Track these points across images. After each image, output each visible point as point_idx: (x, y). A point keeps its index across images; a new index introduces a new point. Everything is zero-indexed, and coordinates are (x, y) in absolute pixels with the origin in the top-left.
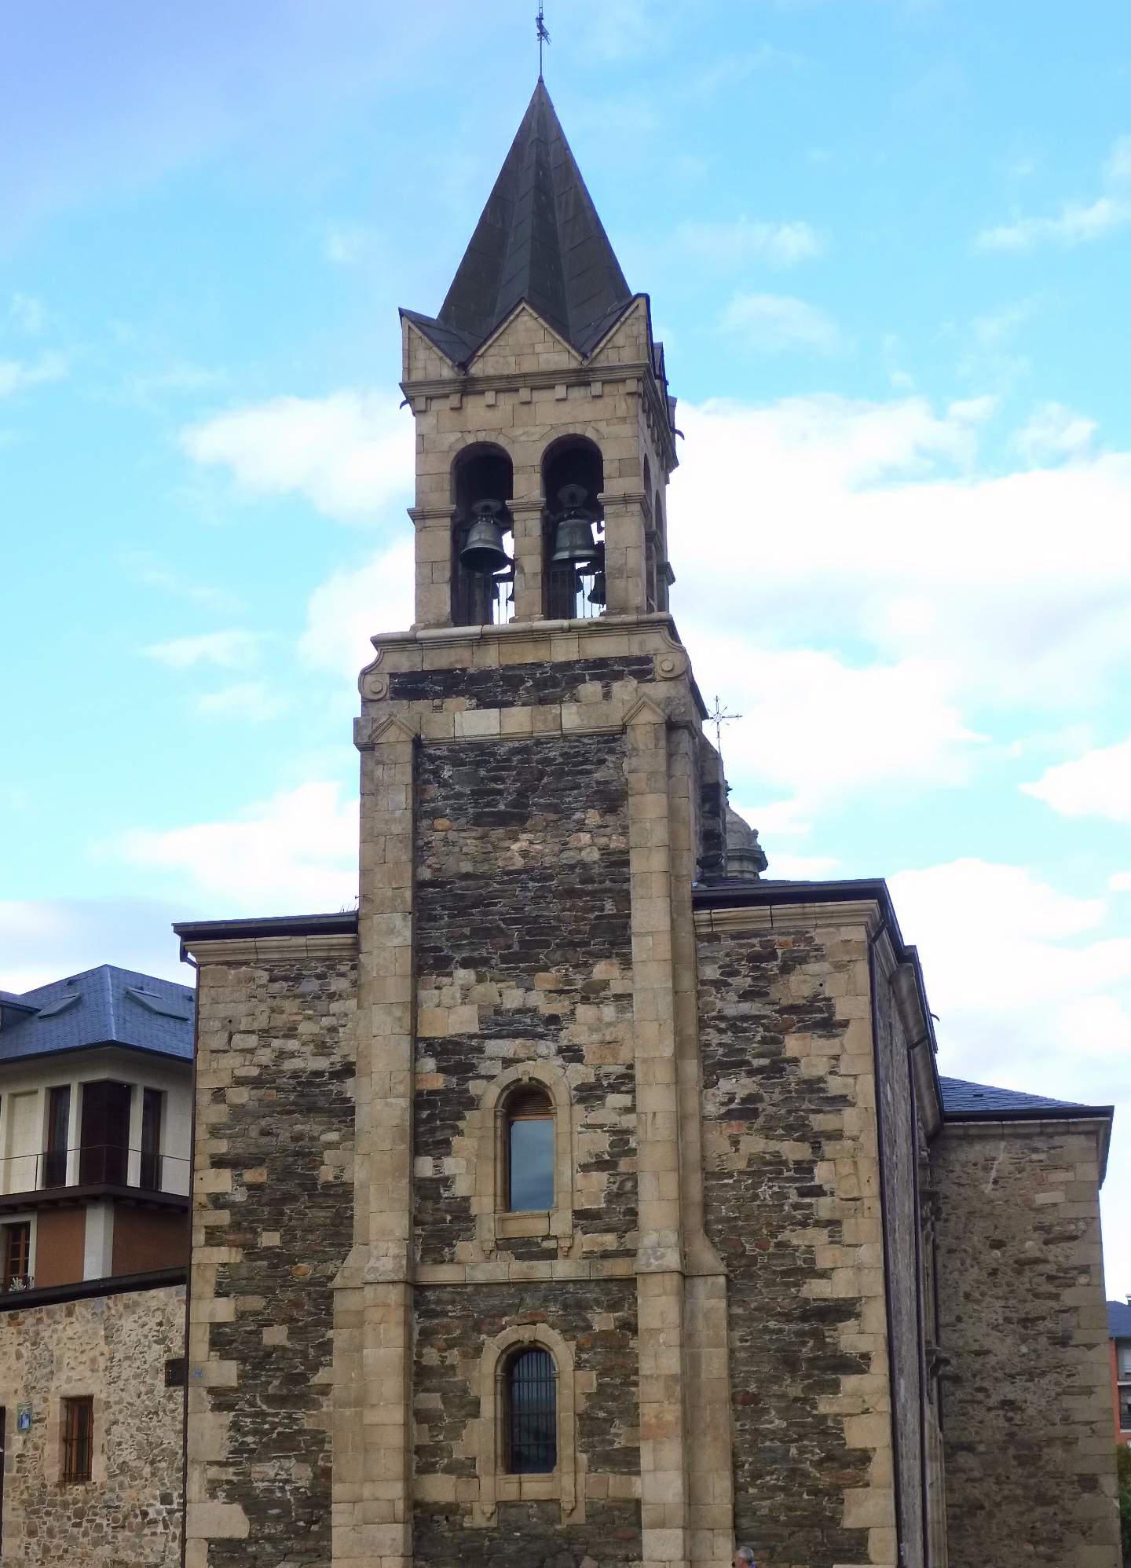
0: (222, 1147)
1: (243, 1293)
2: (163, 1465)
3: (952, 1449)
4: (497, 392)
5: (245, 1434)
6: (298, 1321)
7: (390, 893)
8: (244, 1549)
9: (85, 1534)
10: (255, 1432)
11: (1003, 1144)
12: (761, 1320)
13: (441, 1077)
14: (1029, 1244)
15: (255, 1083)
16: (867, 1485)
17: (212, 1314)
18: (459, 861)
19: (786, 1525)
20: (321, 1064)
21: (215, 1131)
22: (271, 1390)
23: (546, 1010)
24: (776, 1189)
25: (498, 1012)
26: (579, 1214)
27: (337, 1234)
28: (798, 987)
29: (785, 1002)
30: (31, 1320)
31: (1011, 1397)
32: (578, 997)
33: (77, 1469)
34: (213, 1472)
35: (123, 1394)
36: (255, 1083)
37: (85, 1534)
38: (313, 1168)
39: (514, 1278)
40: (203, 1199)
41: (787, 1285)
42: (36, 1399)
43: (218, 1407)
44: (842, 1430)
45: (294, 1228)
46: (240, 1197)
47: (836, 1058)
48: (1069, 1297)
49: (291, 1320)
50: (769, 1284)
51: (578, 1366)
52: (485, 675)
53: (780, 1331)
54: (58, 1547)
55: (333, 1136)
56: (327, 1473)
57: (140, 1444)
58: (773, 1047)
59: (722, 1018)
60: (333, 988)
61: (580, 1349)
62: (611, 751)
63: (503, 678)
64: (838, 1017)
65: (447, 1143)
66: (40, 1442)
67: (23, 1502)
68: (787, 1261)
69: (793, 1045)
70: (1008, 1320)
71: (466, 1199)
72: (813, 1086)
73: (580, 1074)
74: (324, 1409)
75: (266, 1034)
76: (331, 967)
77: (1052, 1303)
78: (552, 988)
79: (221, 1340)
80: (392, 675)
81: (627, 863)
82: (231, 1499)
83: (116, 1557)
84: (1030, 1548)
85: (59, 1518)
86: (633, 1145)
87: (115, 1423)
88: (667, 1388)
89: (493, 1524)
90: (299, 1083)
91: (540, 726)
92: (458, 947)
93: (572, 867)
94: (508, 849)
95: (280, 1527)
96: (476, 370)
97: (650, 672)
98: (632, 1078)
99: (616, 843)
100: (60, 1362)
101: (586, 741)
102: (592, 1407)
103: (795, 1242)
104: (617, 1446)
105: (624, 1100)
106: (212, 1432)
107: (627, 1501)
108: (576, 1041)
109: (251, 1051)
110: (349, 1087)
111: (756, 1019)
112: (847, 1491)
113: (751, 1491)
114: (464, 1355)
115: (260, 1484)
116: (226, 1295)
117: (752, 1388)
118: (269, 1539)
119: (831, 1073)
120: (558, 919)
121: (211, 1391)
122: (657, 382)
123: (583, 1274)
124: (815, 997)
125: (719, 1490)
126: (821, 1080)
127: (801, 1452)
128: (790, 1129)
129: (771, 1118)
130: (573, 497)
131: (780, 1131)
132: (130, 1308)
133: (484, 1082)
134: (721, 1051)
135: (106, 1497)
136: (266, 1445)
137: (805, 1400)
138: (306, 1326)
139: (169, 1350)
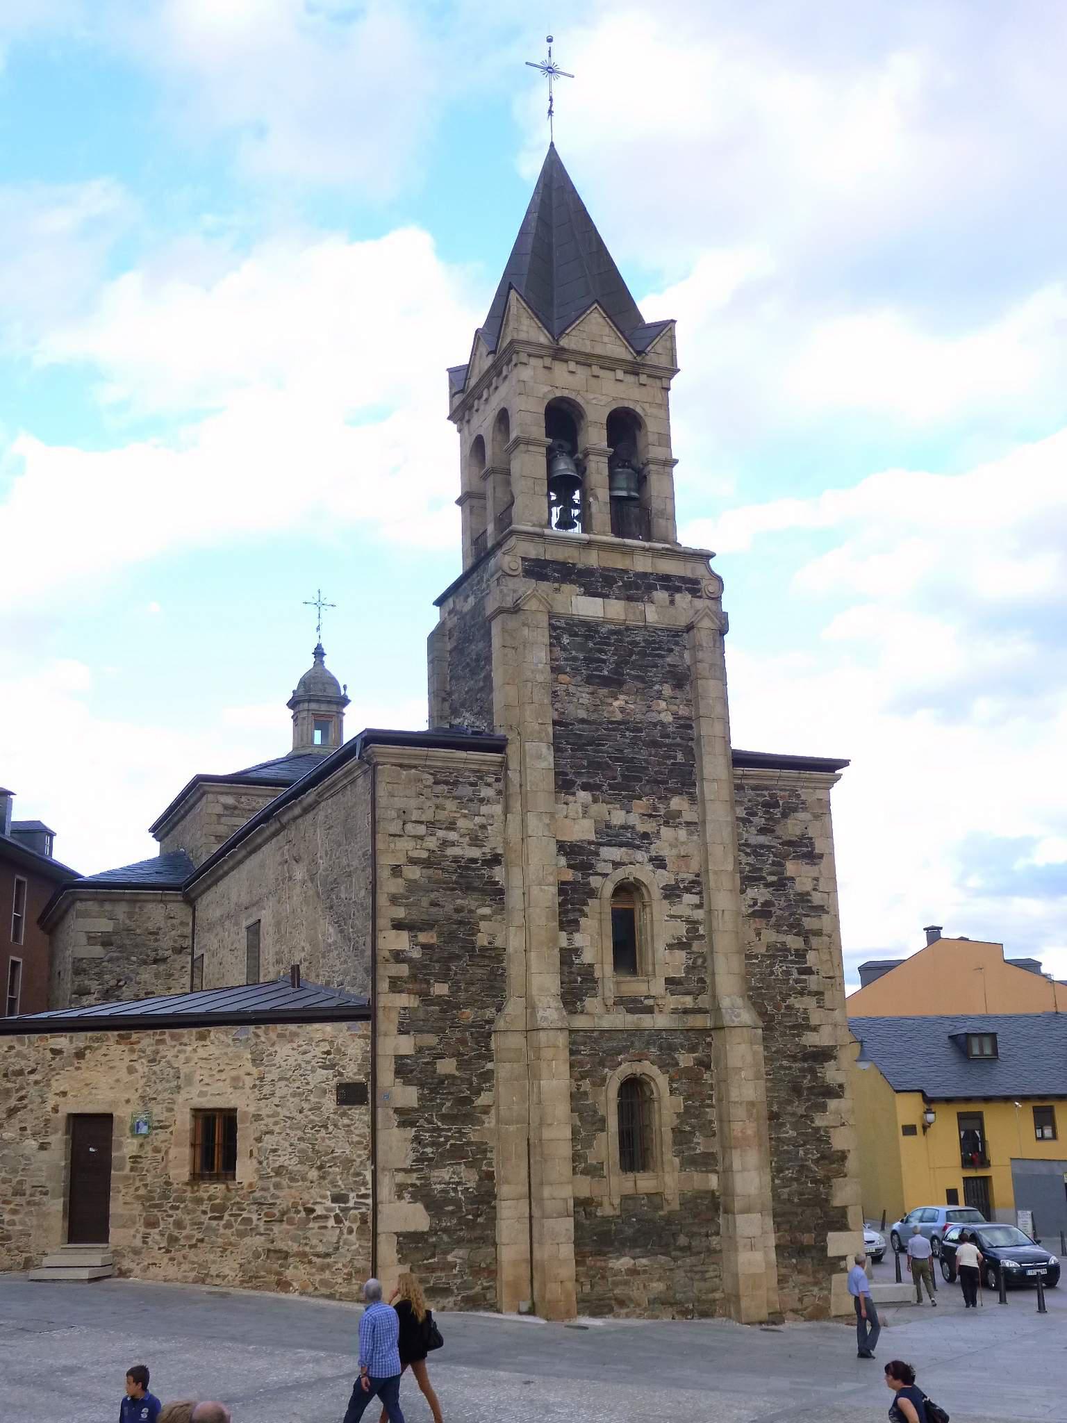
0: (400, 913)
4: (529, 355)
5: (425, 1146)
6: (463, 1055)
7: (537, 727)
8: (426, 1241)
10: (433, 1144)
12: (778, 1060)
13: (571, 871)
15: (426, 863)
16: (845, 1176)
17: (396, 1049)
18: (577, 708)
19: (799, 1205)
20: (475, 853)
21: (394, 900)
23: (641, 828)
25: (608, 826)
26: (669, 981)
27: (492, 987)
34: (400, 1177)
35: (279, 1109)
36: (426, 863)
38: (473, 935)
39: (629, 1027)
41: (794, 1036)
43: (402, 1124)
45: (458, 982)
46: (416, 954)
47: (816, 879)
49: (458, 1055)
50: (783, 1034)
51: (671, 1092)
52: (589, 572)
53: (790, 1068)
54: (188, 1237)
55: (486, 911)
56: (490, 1176)
57: (302, 1151)
58: (779, 869)
59: (747, 845)
60: (482, 795)
61: (671, 1080)
62: (677, 644)
63: (602, 575)
64: (817, 851)
65: (576, 922)
67: (138, 1197)
68: (793, 1019)
71: (591, 966)
72: (803, 897)
74: (486, 1125)
75: (431, 825)
76: (481, 778)
79: (403, 1070)
80: (524, 559)
82: (415, 1199)
83: (271, 1246)
88: (748, 1111)
89: (618, 1212)
90: (459, 867)
91: (631, 617)
92: (578, 774)
93: (655, 725)
94: (611, 705)
95: (455, 1221)
96: (564, 342)
97: (699, 590)
99: (683, 711)
102: (681, 1123)
104: (698, 1151)
106: (397, 1144)
107: (707, 1192)
108: (661, 853)
109: (421, 838)
110: (498, 873)
111: (769, 847)
114: (593, 1084)
115: (438, 1186)
116: (407, 1033)
118: (445, 1230)
119: (815, 889)
121: (396, 1110)
123: (673, 1025)
124: (803, 837)
126: (808, 894)
127: (806, 1154)
128: (791, 926)
129: (780, 918)
131: (785, 928)
133: (600, 878)
135: (257, 1194)
136: (442, 1155)
138: (471, 1059)
139: (341, 1074)
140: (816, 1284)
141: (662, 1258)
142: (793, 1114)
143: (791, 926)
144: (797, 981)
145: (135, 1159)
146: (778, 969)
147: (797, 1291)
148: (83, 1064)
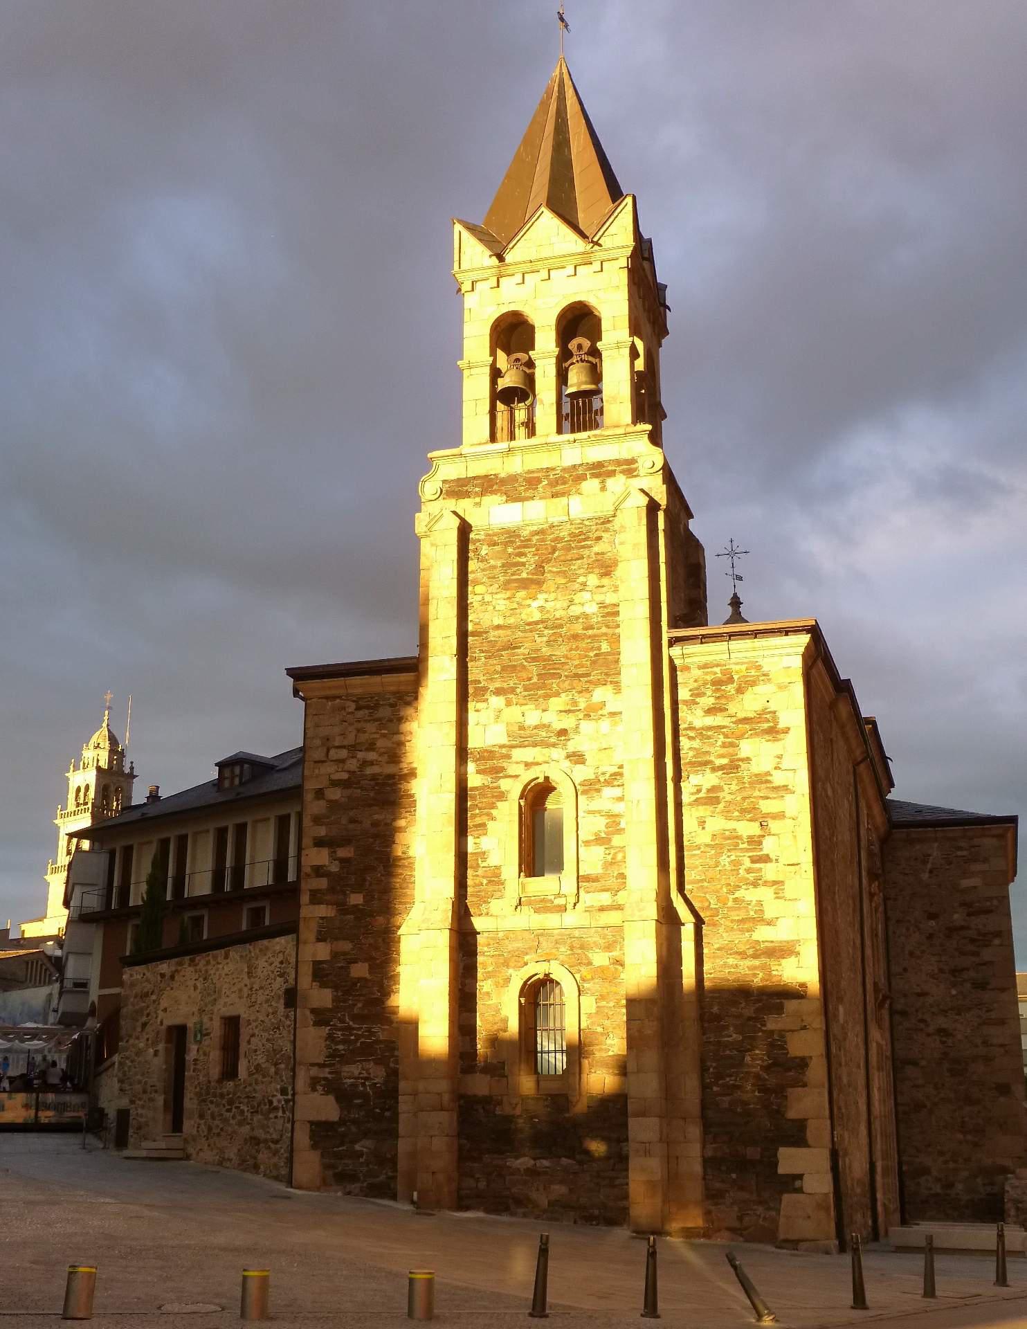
0: (322, 831)
1: (337, 939)
2: (283, 1066)
3: (898, 1065)
9: (234, 1117)
10: (344, 1042)
11: (936, 845)
14: (956, 916)
21: (317, 820)
22: (356, 1011)
23: (557, 726)
24: (733, 858)
25: (522, 728)
28: (749, 704)
29: (741, 715)
30: (203, 962)
31: (944, 1026)
32: (581, 715)
33: (230, 1072)
34: (314, 1071)
37: (234, 1117)
40: (308, 870)
42: (205, 1019)
43: (318, 1023)
44: (785, 1042)
46: (335, 868)
48: (987, 954)
52: (513, 479)
58: (731, 750)
62: (607, 530)
64: (781, 726)
65: (483, 825)
66: (207, 1050)
69: (747, 747)
70: (941, 971)
71: (498, 868)
72: (762, 779)
73: (582, 773)
75: (353, 748)
76: (400, 698)
77: (973, 959)
78: (562, 708)
79: (320, 973)
81: (617, 614)
84: (960, 1136)
85: (217, 1105)
86: (622, 825)
87: (253, 1035)
90: (377, 784)
93: (578, 618)
95: (362, 1113)
97: (635, 470)
98: (621, 775)
99: (610, 598)
100: (220, 991)
101: (587, 523)
103: (748, 898)
105: (617, 792)
106: (313, 1041)
109: (343, 761)
112: (790, 1090)
113: (715, 1089)
114: (497, 985)
115: (348, 1081)
116: (324, 940)
117: (715, 1009)
118: (354, 1122)
120: (566, 657)
121: (313, 1011)
122: (646, 264)
123: (586, 923)
124: (764, 711)
125: (690, 1088)
126: (768, 774)
128: (743, 811)
130: (580, 347)
132: (263, 951)
134: (691, 754)
137: (756, 1019)
140: (760, 1203)
141: (564, 1161)
142: (739, 1016)
143: (743, 811)
144: (749, 871)
145: (195, 1060)
146: (725, 860)
147: (736, 1208)
148: (175, 985)
